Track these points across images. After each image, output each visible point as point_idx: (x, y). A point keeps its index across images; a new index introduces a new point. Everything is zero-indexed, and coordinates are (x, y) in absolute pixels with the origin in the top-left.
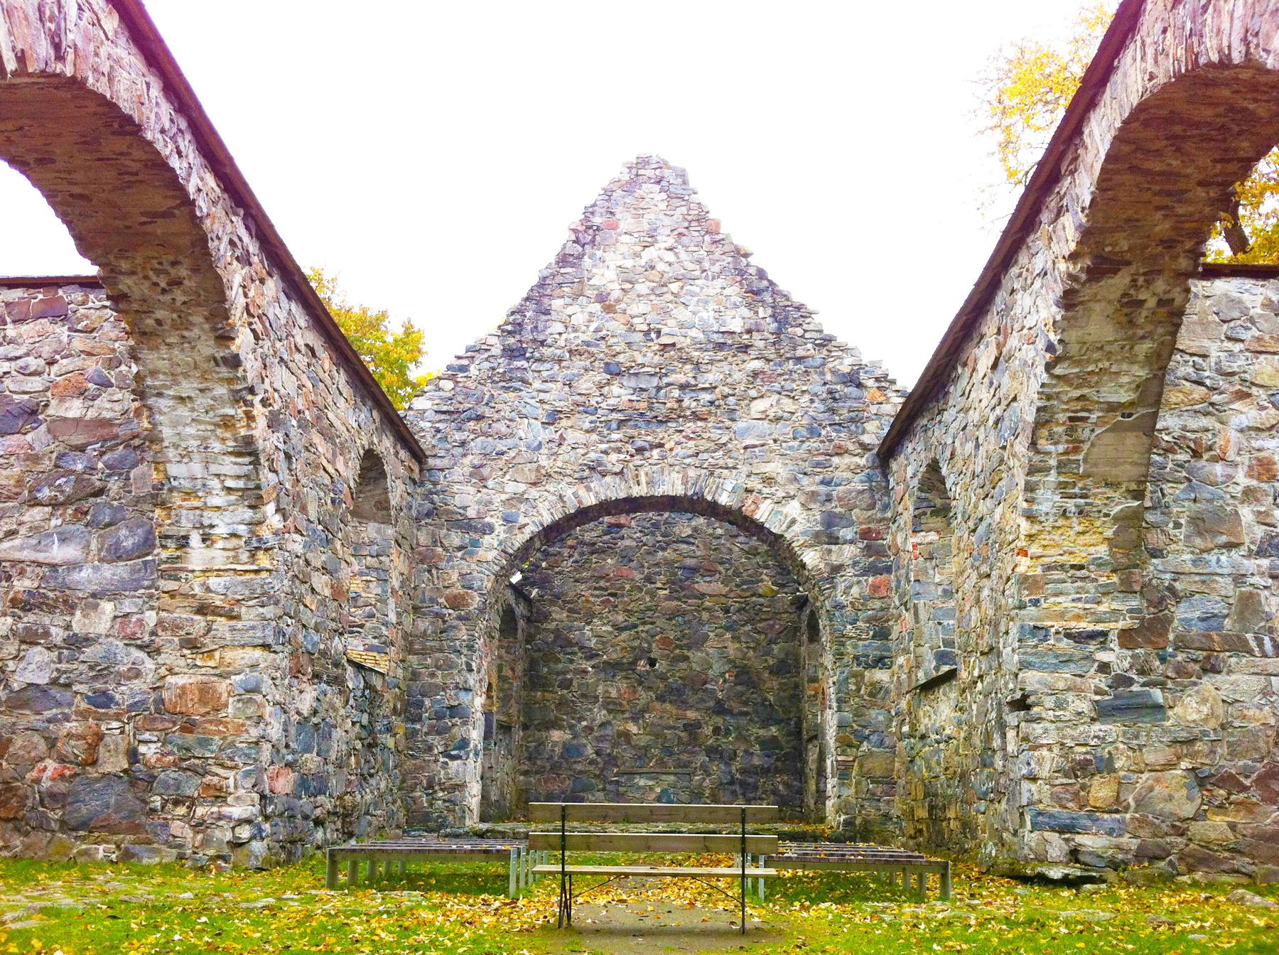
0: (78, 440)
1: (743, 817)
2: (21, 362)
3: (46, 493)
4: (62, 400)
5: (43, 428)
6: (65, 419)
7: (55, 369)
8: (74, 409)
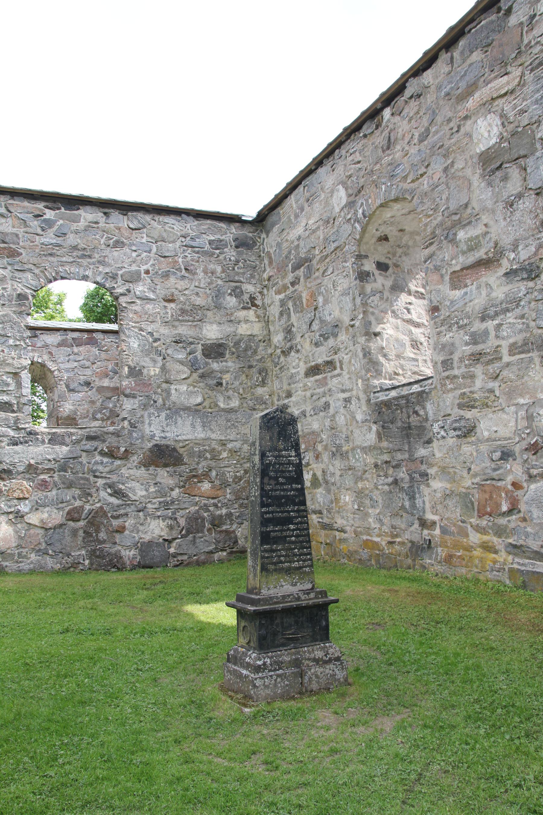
0: (109, 395)
1: (262, 678)
2: (82, 362)
3: (99, 416)
4: (101, 379)
5: (94, 390)
6: (103, 387)
7: (95, 366)
8: (106, 383)
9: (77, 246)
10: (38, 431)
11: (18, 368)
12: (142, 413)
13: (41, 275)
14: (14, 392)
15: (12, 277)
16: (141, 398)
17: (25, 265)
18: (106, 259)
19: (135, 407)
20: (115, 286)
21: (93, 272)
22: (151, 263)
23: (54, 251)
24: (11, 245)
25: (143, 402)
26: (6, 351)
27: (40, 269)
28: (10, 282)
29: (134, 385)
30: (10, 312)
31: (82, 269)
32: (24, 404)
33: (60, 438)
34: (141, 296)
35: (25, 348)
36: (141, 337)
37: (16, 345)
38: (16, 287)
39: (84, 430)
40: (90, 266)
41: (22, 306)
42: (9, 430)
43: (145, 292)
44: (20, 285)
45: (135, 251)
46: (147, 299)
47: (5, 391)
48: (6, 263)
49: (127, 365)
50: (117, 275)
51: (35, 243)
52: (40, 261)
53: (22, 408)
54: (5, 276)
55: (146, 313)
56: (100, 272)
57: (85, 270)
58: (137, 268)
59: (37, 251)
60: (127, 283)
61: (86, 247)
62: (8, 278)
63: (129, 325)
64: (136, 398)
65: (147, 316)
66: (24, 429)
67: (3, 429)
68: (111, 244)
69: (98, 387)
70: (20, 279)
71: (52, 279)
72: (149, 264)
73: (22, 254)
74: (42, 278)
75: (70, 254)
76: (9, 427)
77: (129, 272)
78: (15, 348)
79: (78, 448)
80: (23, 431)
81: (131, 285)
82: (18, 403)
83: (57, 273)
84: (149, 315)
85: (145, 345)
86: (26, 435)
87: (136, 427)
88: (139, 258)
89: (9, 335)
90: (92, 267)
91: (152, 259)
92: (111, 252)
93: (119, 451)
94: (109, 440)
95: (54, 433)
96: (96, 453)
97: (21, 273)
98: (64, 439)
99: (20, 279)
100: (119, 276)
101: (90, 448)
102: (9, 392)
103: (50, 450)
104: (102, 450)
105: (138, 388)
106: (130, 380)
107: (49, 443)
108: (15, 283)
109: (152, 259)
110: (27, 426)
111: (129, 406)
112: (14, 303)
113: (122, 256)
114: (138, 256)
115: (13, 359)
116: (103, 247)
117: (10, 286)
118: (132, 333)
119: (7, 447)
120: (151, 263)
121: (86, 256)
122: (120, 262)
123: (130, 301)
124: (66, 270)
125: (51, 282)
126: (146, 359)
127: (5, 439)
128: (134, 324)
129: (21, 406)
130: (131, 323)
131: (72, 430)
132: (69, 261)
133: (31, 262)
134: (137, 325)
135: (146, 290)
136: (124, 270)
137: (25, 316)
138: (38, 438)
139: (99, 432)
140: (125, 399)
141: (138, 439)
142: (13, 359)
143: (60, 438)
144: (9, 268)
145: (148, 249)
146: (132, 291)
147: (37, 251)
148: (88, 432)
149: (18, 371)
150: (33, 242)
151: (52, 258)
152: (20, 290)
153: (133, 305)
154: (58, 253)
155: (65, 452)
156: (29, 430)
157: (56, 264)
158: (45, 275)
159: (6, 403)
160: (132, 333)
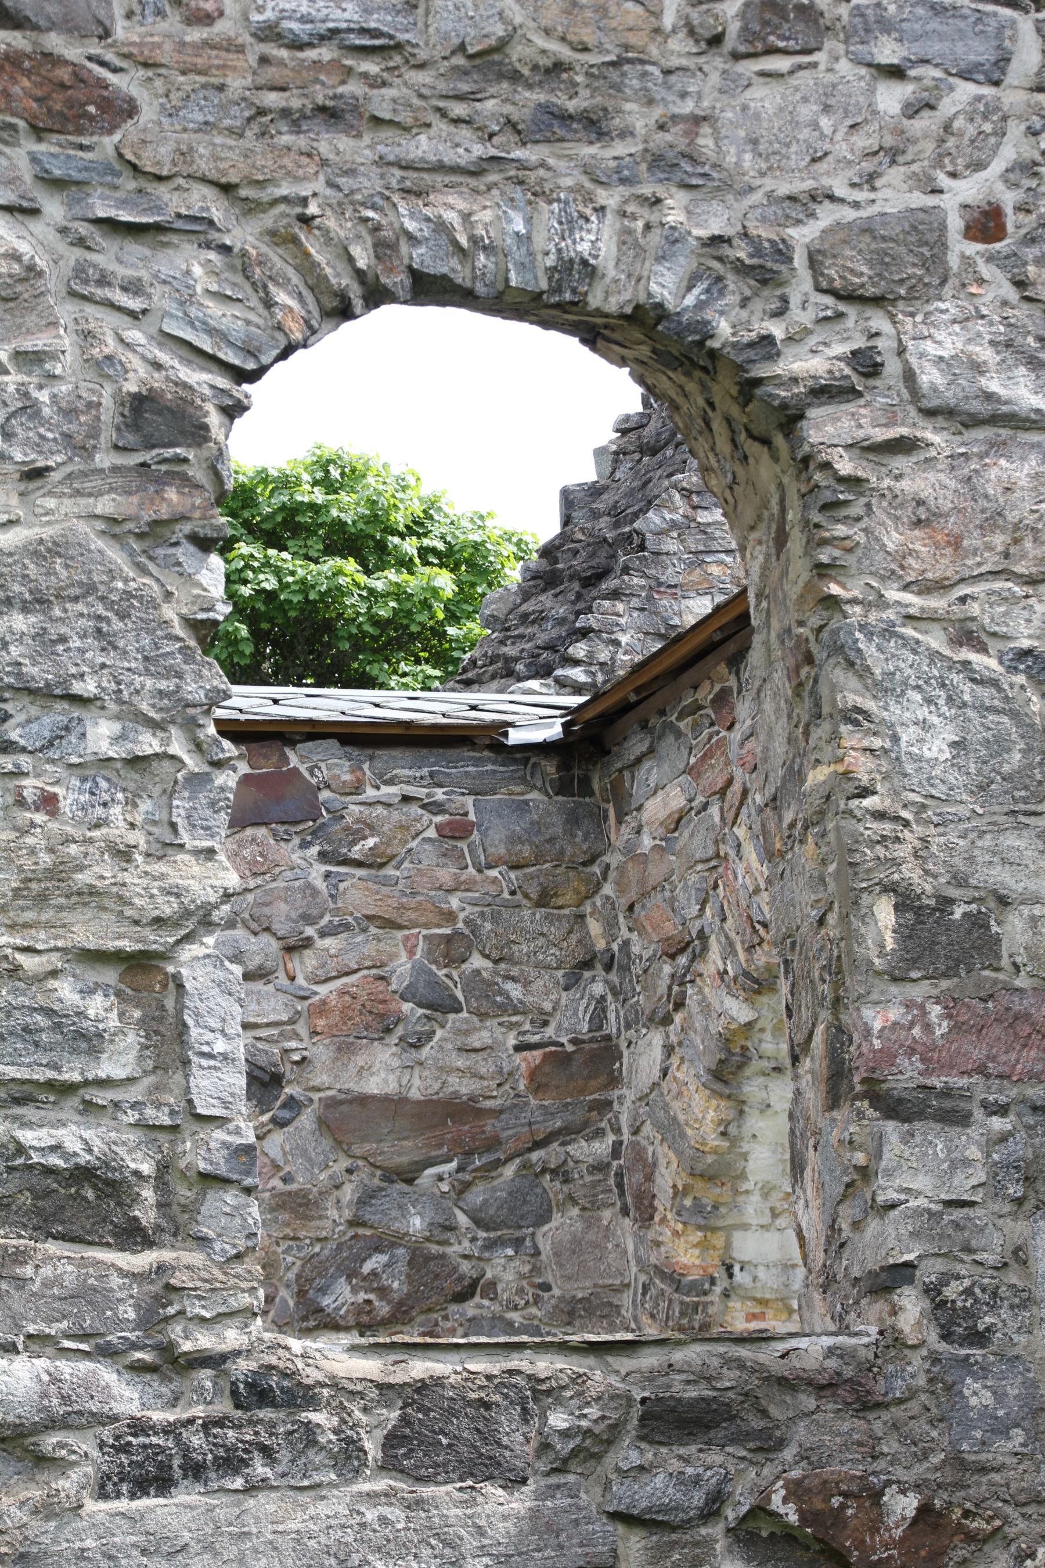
6: (363, 1100)
9: (501, 46)
10: (311, 1375)
11: (158, 922)
12: (1018, 1229)
13: (278, 259)
14: (134, 1093)
15: (80, 271)
16: (997, 1124)
17: (162, 191)
18: (706, 142)
19: (962, 1185)
20: (777, 330)
21: (625, 239)
22: (1007, 154)
23: (353, 88)
24: (55, 42)
25: (1019, 1148)
26: (68, 799)
27: (269, 219)
28: (66, 312)
29: (942, 1028)
30: (83, 527)
31: (548, 215)
32: (210, 1180)
33: (462, 1427)
34: (950, 397)
35: (197, 781)
36: (967, 691)
37: (136, 762)
38: (111, 346)
39: (625, 1364)
40: (603, 197)
41: (162, 481)
42: (107, 1375)
43: (978, 368)
44: (134, 335)
45: (896, 72)
46: (994, 420)
47: (67, 1089)
48: (26, 172)
49: (889, 888)
50: (782, 252)
51: (222, 28)
52: (264, 162)
53: (191, 1209)
54: (32, 271)
55: (993, 520)
56: (674, 238)
57: (570, 224)
58: (919, 200)
59: (237, 84)
60: (851, 310)
61: (565, 53)
62: (52, 283)
63: (881, 603)
64: (963, 1119)
65: (999, 540)
66: (215, 1361)
67: (66, 1367)
68: (734, 28)
69: (331, 1104)
70: (132, 287)
71: (355, 293)
72: (997, 166)
73: (131, 110)
74: (284, 283)
75: (459, 109)
76: (107, 1352)
77: (867, 229)
78: (132, 776)
79: (589, 1498)
80: (205, 1377)
81: (879, 321)
82: (164, 1168)
83: (383, 248)
84: (1017, 533)
85: (999, 745)
86: (223, 1407)
87: (979, 1338)
88: (924, 124)
89: (88, 687)
90: (610, 198)
91: (1015, 130)
92: (731, 86)
93: (876, 1525)
94: (801, 1433)
95: (422, 1387)
96: (715, 1531)
97: (135, 249)
98: (489, 1435)
99: (132, 287)
100: (799, 260)
101: (673, 1494)
102: (102, 1097)
103: (396, 1513)
104: (760, 1511)
105: (978, 1054)
106: (918, 991)
107: (389, 1466)
108: (105, 322)
109: (1015, 130)
110: (232, 1338)
111: (921, 1182)
112: (104, 460)
113: (806, 112)
114: (913, 109)
115: (123, 854)
116: (679, 45)
117: (67, 342)
118: (906, 664)
119: (91, 1506)
120: (1007, 154)
121: (565, 118)
122: (797, 158)
123: (881, 435)
124: (441, 227)
125: (344, 312)
126: (1011, 840)
127: (84, 1443)
128: (915, 602)
129: (184, 1193)
130: (893, 594)
131: (544, 1365)
132: (459, 157)
133: (203, 166)
134: (937, 603)
135: (986, 354)
136: (827, 216)
137: (185, 553)
138: (309, 1427)
139: (730, 1378)
140: (892, 1129)
141: (1003, 1430)
142: (123, 854)
143: (462, 1427)
144: (54, 208)
145: (980, 52)
146: (892, 368)
147: (237, 84)
148: (649, 1377)
149: (157, 940)
150: (206, 19)
151: (344, 143)
152: (142, 370)
153: (900, 463)
154: (382, 103)
155: (501, 1530)
156: (244, 1366)
157: (369, 183)
158: (307, 267)
159: (83, 1174)
160: (906, 664)
